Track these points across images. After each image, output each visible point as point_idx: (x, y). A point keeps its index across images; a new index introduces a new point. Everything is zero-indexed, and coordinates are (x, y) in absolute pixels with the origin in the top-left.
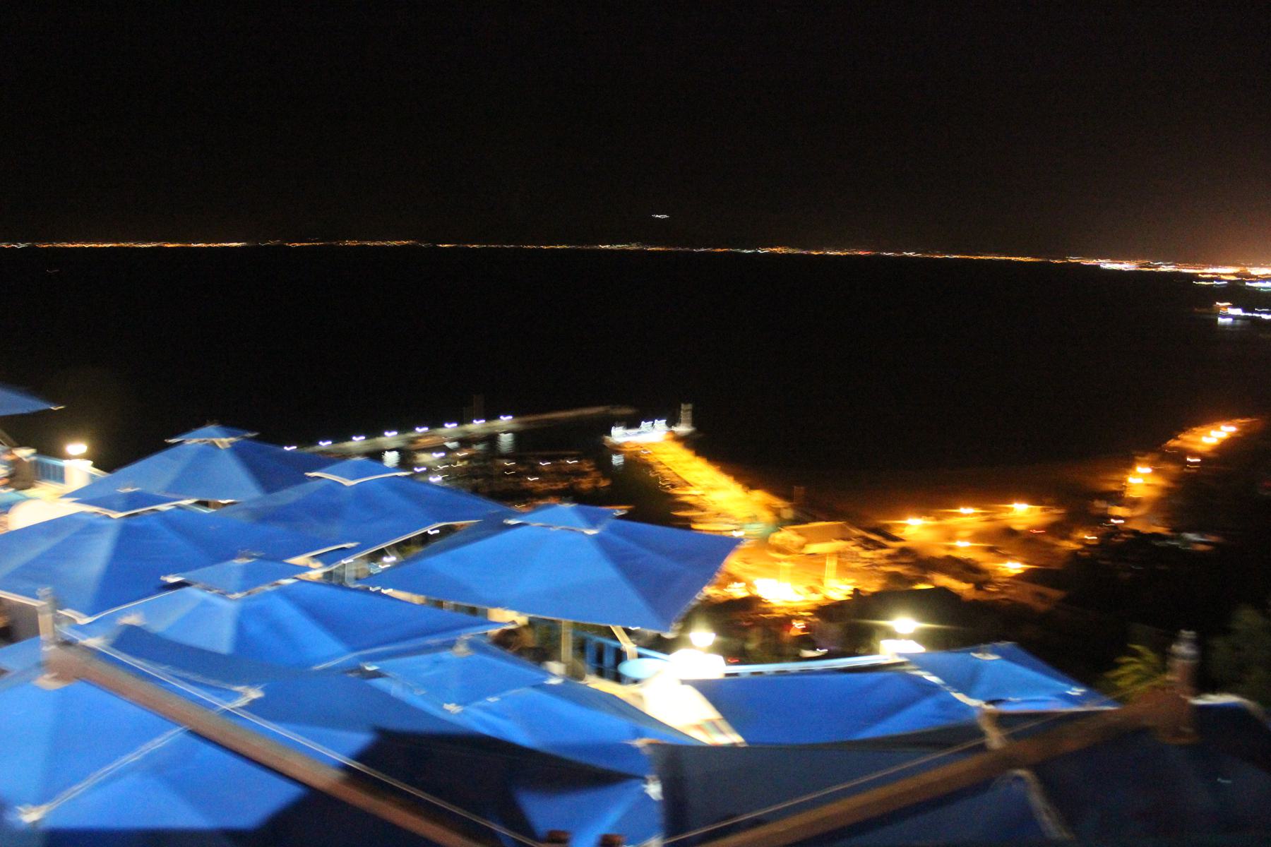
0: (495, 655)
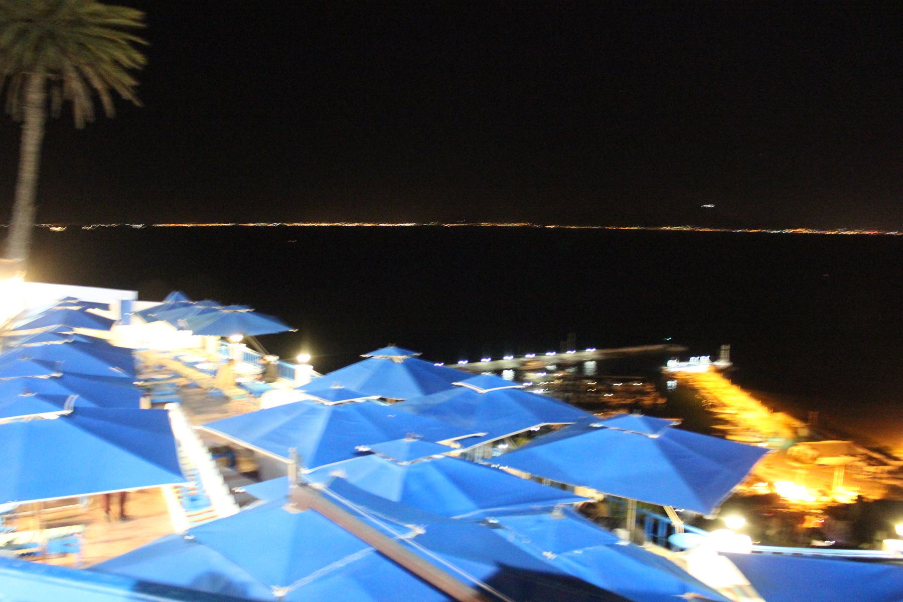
0: (579, 520)
